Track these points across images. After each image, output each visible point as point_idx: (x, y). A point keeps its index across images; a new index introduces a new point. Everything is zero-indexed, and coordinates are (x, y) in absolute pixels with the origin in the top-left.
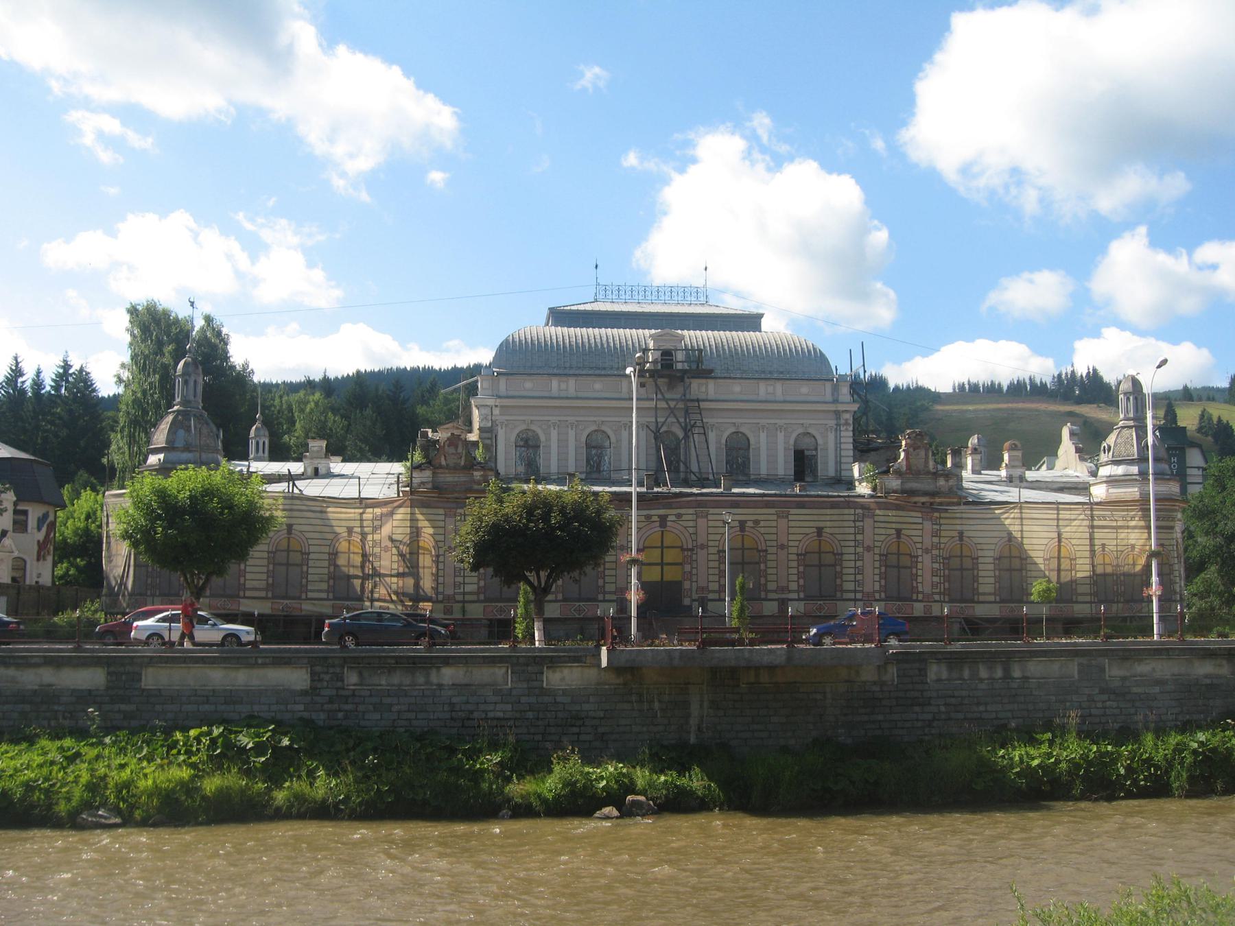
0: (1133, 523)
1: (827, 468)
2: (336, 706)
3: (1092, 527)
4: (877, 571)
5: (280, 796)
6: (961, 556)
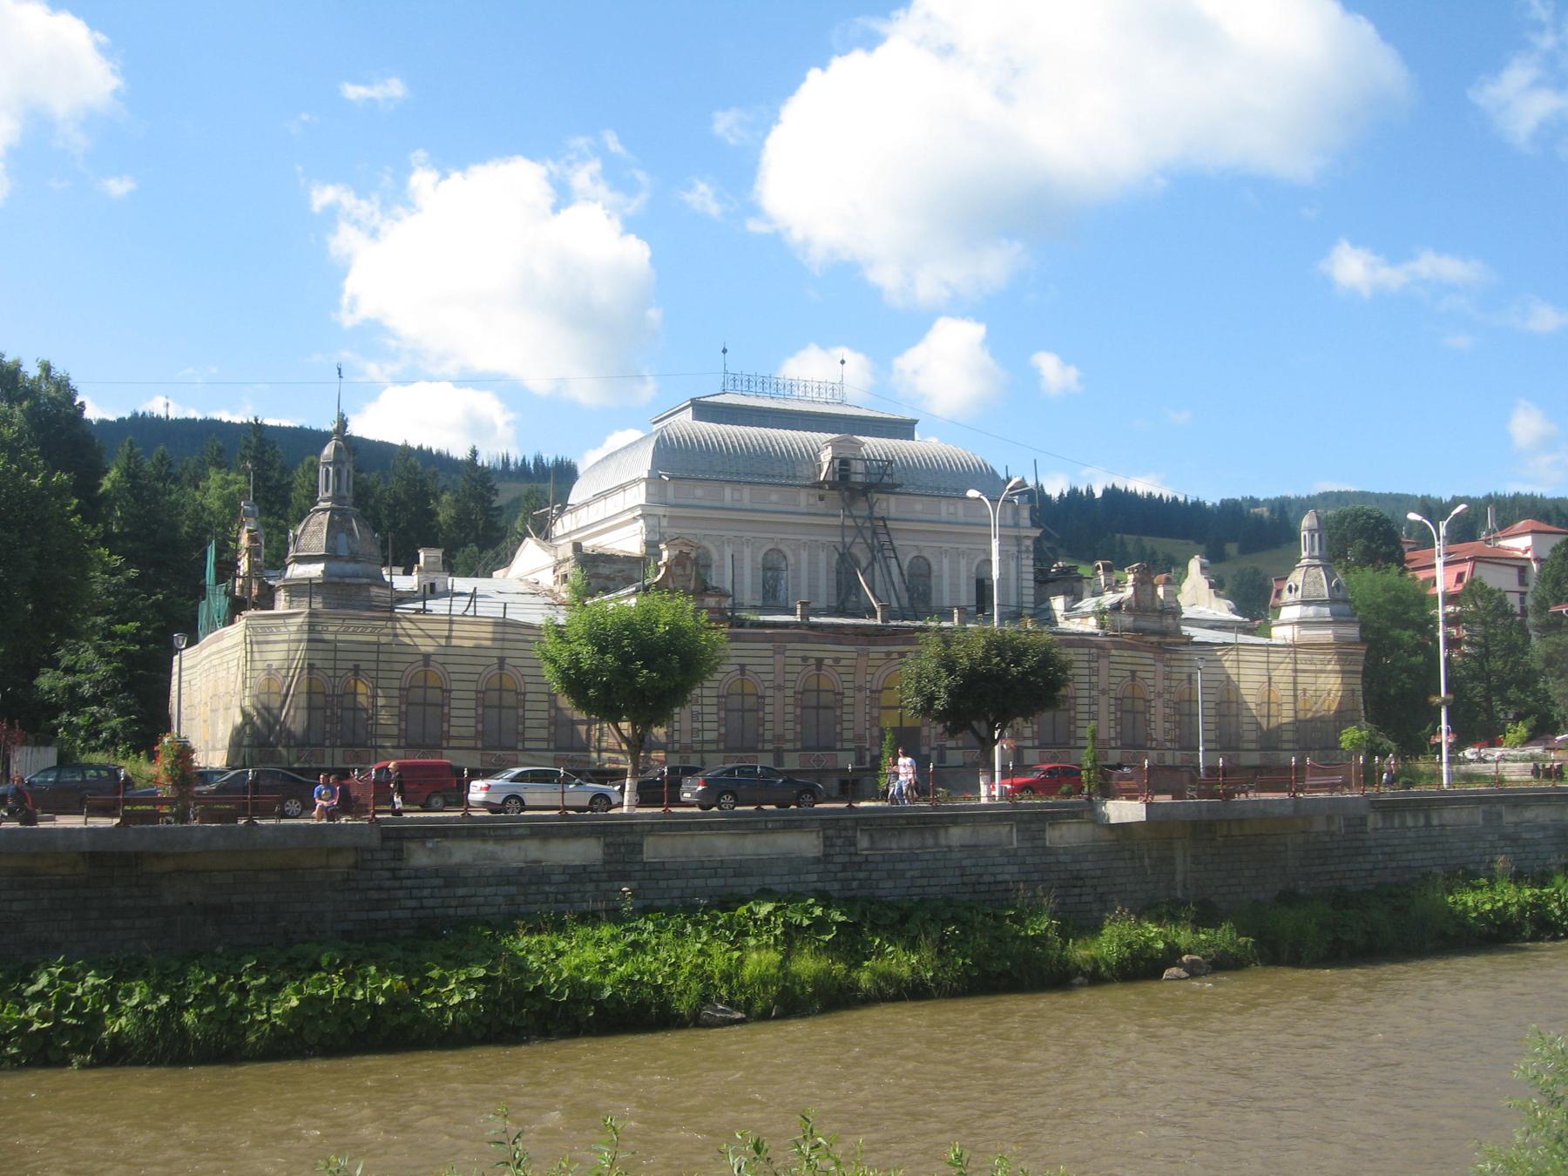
0: (1329, 667)
3: (1296, 671)
6: (500, 690)
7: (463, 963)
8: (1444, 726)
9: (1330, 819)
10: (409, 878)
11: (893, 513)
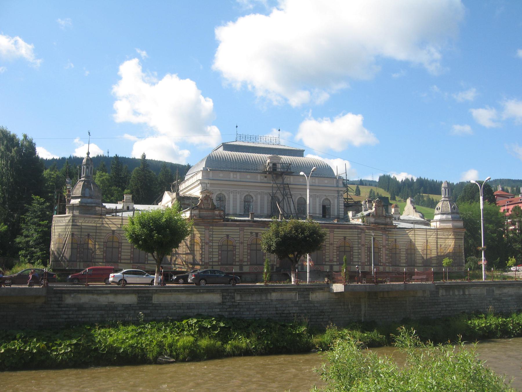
0: (450, 237)
1: (334, 211)
2: (232, 309)
3: (437, 238)
4: (366, 254)
5: (228, 347)
7: (71, 338)
8: (483, 258)
9: (424, 291)
10: (64, 307)
11: (292, 182)
